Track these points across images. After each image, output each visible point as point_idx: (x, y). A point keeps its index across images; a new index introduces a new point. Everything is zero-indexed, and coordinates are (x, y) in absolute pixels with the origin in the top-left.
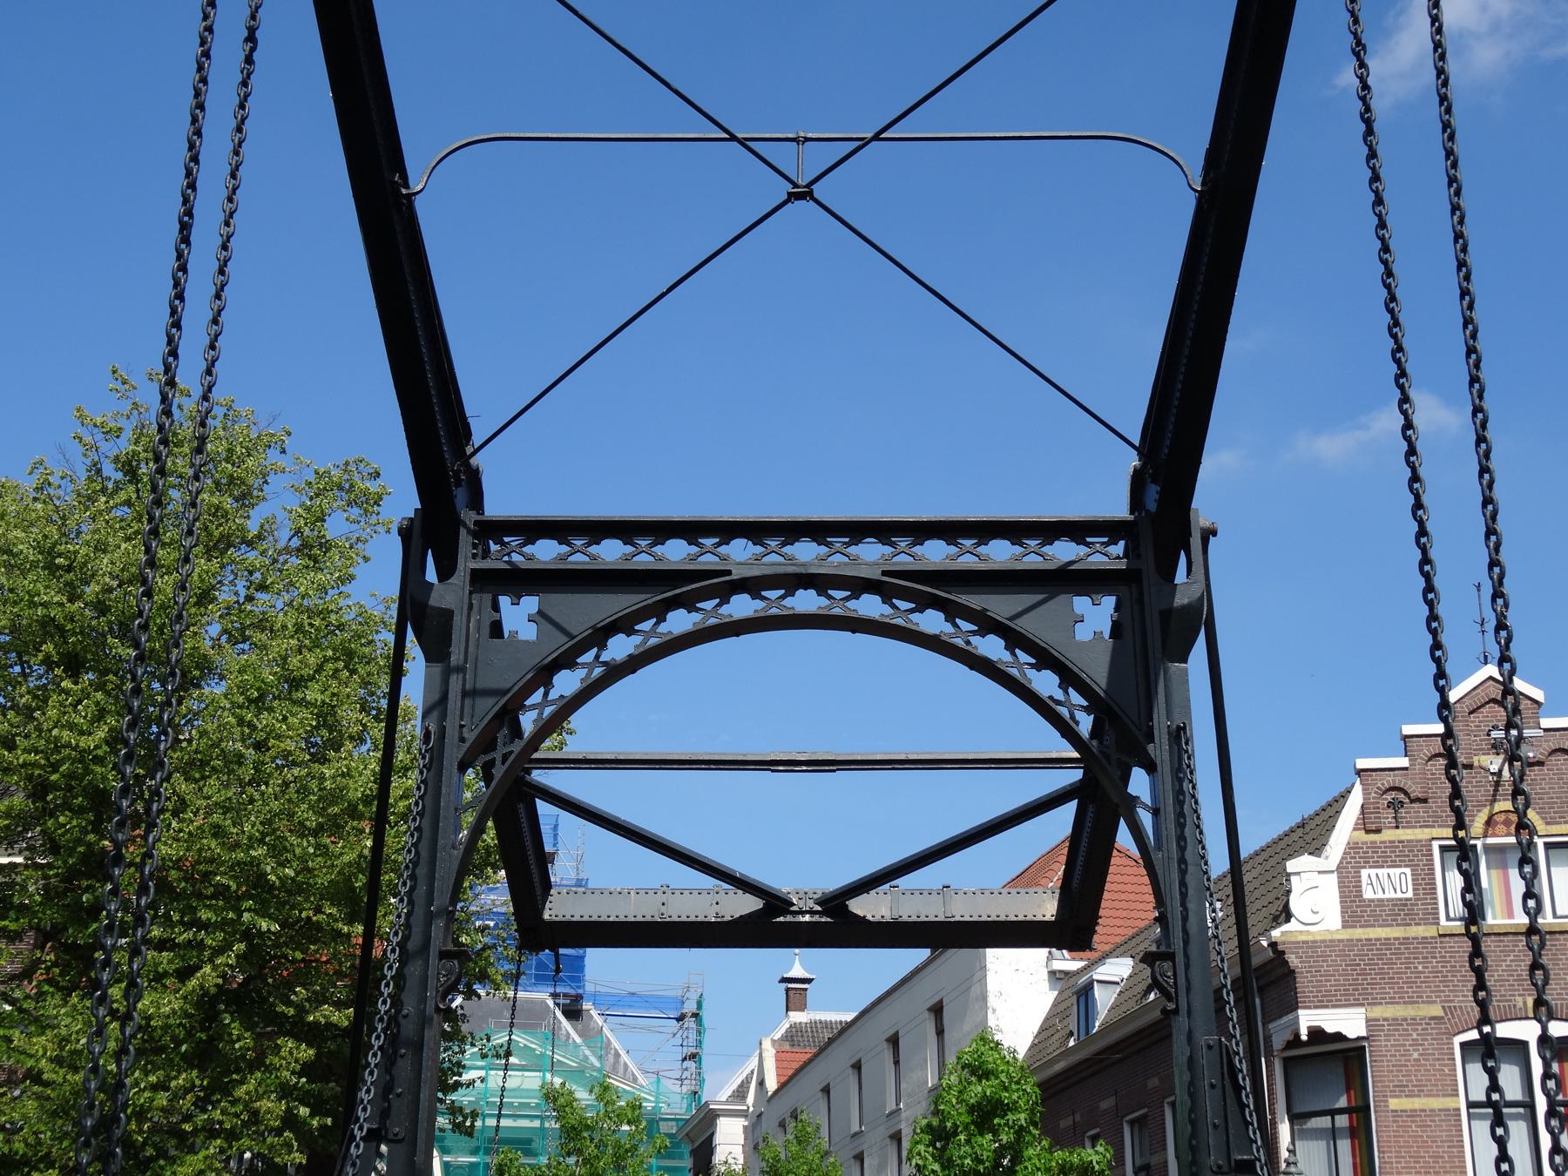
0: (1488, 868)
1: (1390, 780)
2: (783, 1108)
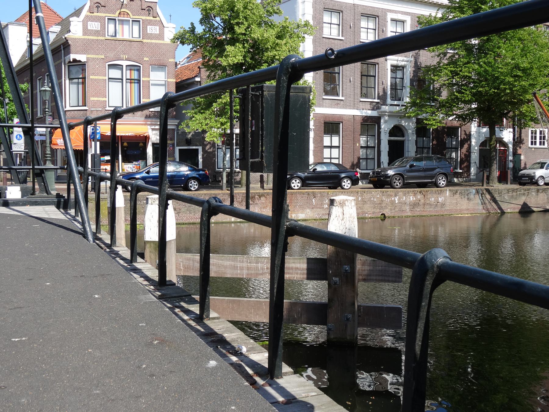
0: (119, 24)
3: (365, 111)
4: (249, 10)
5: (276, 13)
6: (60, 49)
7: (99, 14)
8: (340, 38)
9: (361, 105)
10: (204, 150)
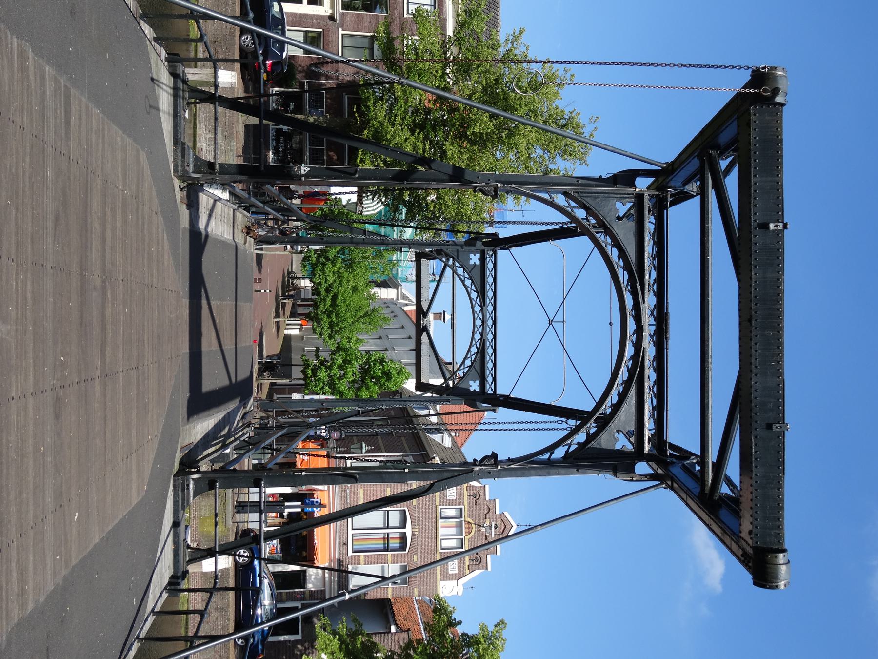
0: (456, 522)
1: (482, 494)
2: (398, 312)
6: (421, 449)
7: (466, 498)
10: (297, 642)
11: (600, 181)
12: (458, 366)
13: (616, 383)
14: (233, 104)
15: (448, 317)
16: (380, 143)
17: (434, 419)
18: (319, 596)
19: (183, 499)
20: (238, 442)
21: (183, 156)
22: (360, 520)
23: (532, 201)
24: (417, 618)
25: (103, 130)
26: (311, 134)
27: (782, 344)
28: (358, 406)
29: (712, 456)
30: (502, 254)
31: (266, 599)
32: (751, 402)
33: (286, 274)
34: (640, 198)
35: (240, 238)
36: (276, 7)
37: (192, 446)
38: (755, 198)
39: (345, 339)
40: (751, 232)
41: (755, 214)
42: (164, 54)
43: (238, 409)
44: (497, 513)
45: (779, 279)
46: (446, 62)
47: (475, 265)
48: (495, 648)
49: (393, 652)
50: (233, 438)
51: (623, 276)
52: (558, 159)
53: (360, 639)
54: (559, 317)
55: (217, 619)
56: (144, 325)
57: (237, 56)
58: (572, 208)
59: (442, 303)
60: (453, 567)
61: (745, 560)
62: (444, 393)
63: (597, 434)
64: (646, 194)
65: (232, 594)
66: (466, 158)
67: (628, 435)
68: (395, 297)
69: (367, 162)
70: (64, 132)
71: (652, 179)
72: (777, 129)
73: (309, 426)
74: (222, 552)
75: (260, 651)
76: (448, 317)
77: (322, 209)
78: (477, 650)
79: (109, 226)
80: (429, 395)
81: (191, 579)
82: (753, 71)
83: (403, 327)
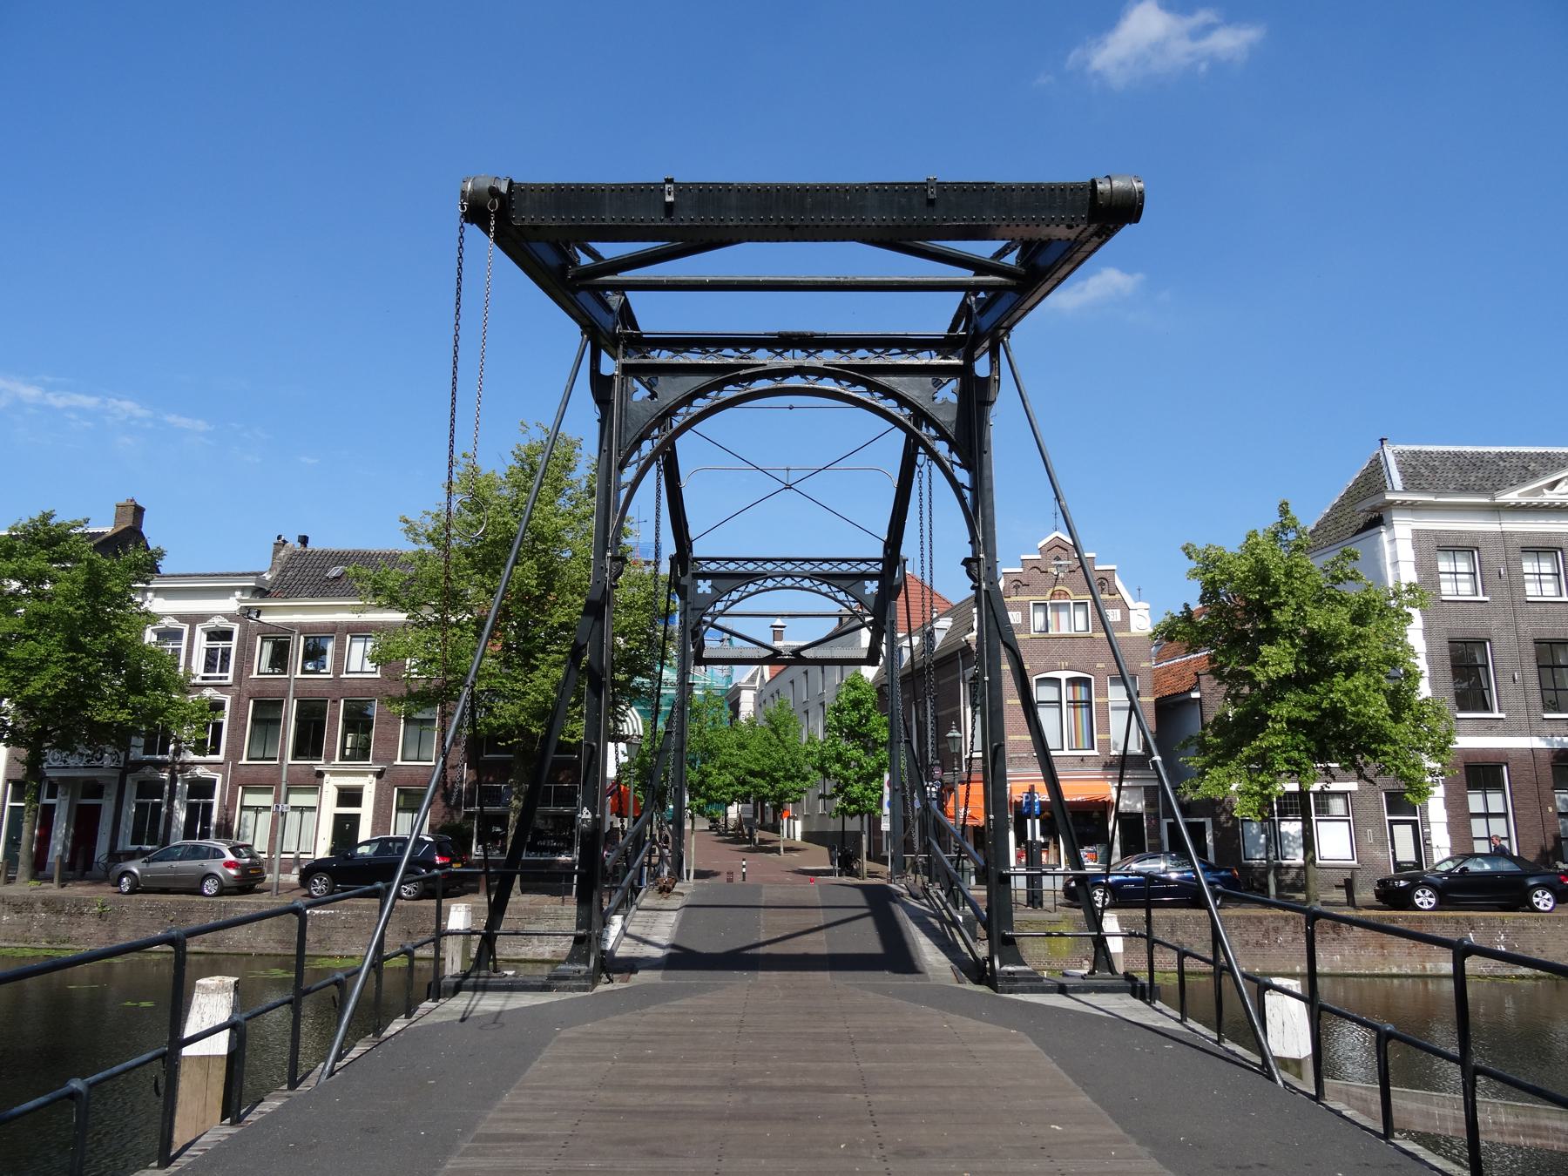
1: (1015, 577)
2: (773, 688)
3: (1559, 739)
4: (1296, 578)
5: (1351, 579)
7: (1019, 598)
8: (1481, 598)
9: (1547, 728)
10: (1217, 826)
11: (604, 421)
12: (844, 608)
13: (870, 401)
14: (497, 909)
15: (778, 622)
16: (551, 711)
17: (916, 640)
18: (1153, 795)
19: (1028, 980)
20: (949, 905)
21: (566, 978)
22: (1052, 740)
23: (629, 514)
24: (1180, 663)
25: (531, 1088)
26: (539, 803)
27: (822, 186)
28: (899, 742)
29: (967, 276)
30: (698, 551)
31: (1158, 866)
32: (899, 226)
33: (720, 838)
34: (627, 370)
35: (675, 902)
36: (364, 850)
37: (956, 967)
38: (633, 220)
39: (808, 760)
40: (677, 226)
41: (653, 220)
42: (428, 1004)
43: (905, 905)
44: (1039, 557)
45: (739, 190)
46: (444, 624)
47: (711, 586)
48: (1220, 559)
49: (1227, 695)
50: (944, 911)
51: (730, 392)
52: (574, 476)
53: (1210, 738)
54: (782, 476)
55: (1186, 933)
56: (796, 1033)
57: (433, 903)
58: (640, 458)
59: (760, 630)
60: (1114, 615)
61: (1105, 234)
62: (881, 626)
63: (938, 427)
64: (623, 361)
65: (1155, 913)
66: (571, 597)
67: (938, 385)
68: (753, 692)
69: (574, 729)
70: (537, 1143)
71: (603, 352)
72: (543, 190)
73: (926, 808)
74: (1099, 928)
75: (1229, 874)
76: (778, 622)
77: (636, 790)
78: (1222, 582)
79: (661, 1082)
80: (884, 648)
81: (1134, 968)
82: (466, 221)
83: (792, 682)
